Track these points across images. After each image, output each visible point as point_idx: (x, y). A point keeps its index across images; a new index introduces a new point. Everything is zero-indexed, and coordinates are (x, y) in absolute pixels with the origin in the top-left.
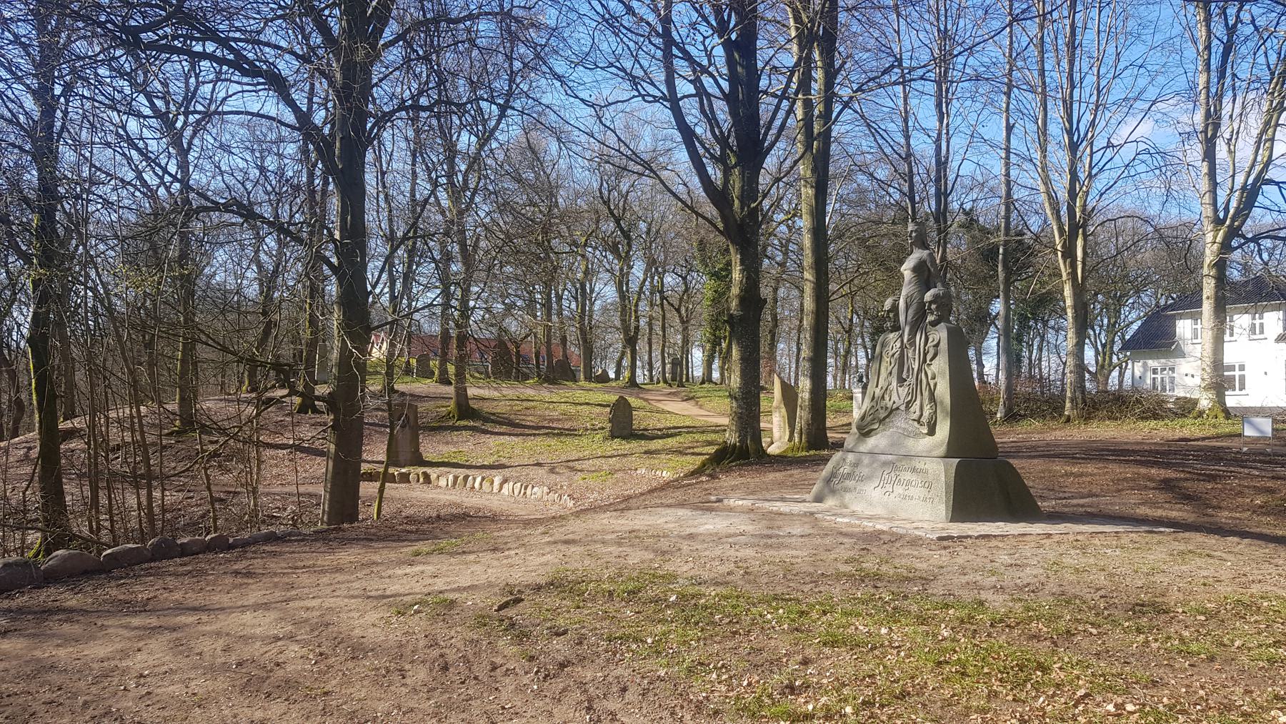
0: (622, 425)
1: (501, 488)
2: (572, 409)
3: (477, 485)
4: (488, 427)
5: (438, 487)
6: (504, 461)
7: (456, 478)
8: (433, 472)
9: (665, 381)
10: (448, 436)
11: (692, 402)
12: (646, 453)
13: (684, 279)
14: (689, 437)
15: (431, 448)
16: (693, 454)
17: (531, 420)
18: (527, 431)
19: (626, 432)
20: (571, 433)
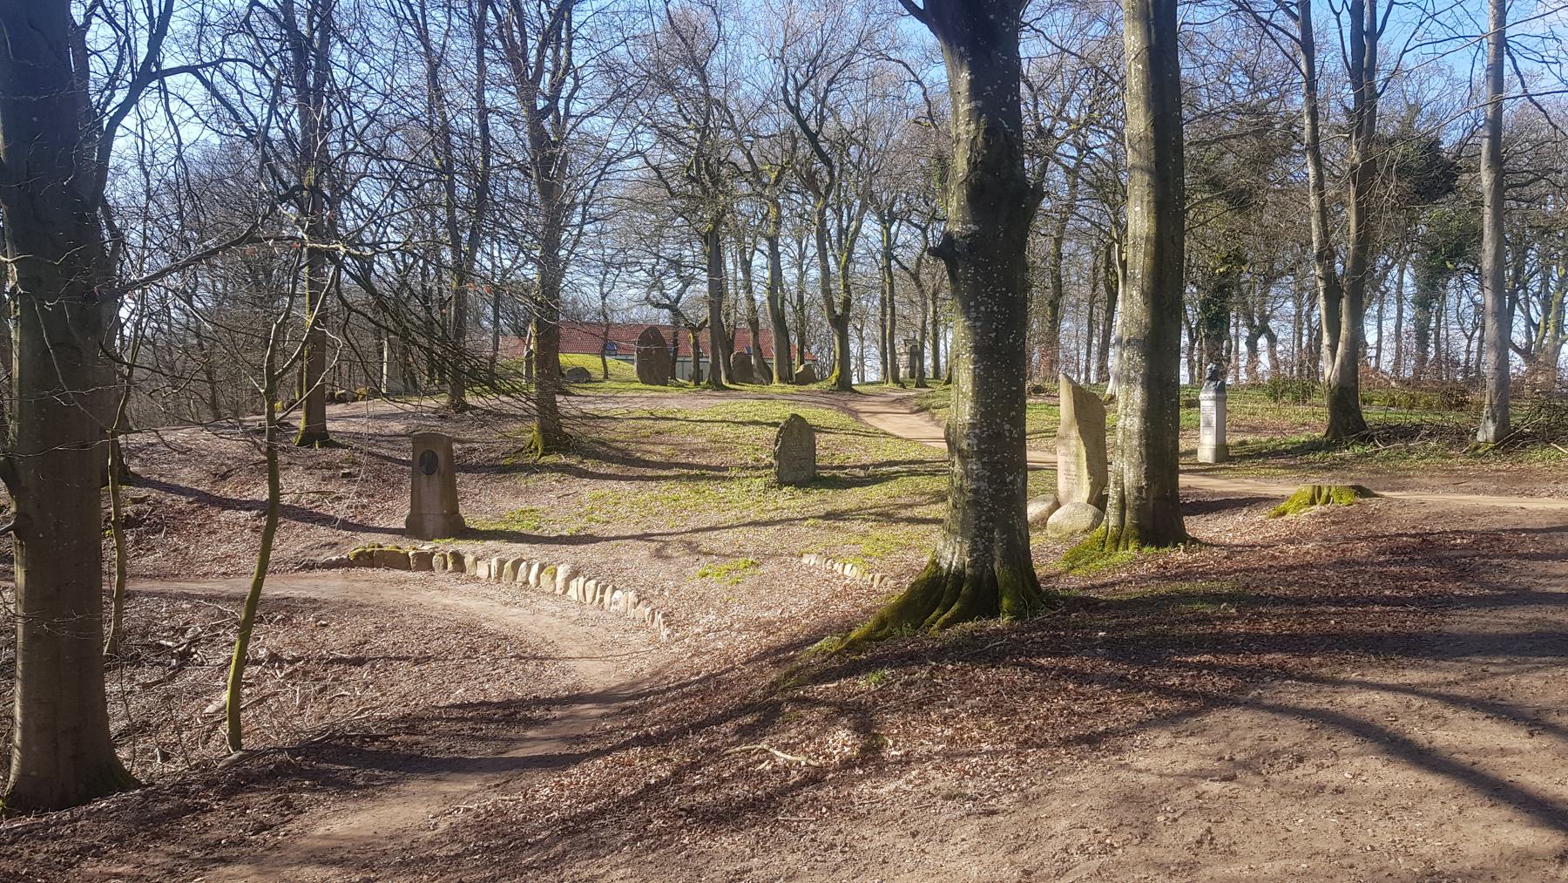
0: (798, 461)
1: (566, 588)
2: (729, 432)
3: (532, 579)
4: (589, 465)
5: (476, 579)
6: (596, 529)
7: (502, 563)
8: (466, 547)
9: (896, 380)
10: (522, 481)
11: (925, 415)
12: (828, 516)
13: (924, 231)
14: (909, 483)
15: (483, 503)
16: (911, 521)
17: (659, 452)
18: (649, 472)
19: (803, 475)
20: (717, 474)
